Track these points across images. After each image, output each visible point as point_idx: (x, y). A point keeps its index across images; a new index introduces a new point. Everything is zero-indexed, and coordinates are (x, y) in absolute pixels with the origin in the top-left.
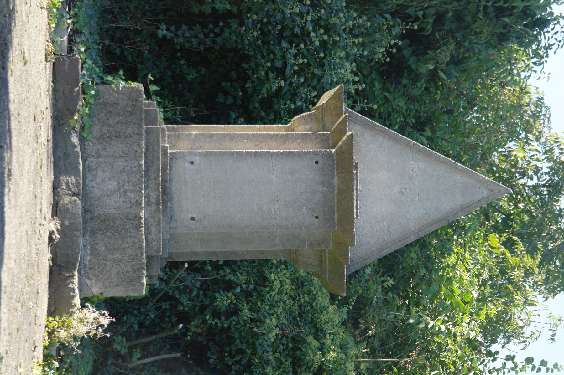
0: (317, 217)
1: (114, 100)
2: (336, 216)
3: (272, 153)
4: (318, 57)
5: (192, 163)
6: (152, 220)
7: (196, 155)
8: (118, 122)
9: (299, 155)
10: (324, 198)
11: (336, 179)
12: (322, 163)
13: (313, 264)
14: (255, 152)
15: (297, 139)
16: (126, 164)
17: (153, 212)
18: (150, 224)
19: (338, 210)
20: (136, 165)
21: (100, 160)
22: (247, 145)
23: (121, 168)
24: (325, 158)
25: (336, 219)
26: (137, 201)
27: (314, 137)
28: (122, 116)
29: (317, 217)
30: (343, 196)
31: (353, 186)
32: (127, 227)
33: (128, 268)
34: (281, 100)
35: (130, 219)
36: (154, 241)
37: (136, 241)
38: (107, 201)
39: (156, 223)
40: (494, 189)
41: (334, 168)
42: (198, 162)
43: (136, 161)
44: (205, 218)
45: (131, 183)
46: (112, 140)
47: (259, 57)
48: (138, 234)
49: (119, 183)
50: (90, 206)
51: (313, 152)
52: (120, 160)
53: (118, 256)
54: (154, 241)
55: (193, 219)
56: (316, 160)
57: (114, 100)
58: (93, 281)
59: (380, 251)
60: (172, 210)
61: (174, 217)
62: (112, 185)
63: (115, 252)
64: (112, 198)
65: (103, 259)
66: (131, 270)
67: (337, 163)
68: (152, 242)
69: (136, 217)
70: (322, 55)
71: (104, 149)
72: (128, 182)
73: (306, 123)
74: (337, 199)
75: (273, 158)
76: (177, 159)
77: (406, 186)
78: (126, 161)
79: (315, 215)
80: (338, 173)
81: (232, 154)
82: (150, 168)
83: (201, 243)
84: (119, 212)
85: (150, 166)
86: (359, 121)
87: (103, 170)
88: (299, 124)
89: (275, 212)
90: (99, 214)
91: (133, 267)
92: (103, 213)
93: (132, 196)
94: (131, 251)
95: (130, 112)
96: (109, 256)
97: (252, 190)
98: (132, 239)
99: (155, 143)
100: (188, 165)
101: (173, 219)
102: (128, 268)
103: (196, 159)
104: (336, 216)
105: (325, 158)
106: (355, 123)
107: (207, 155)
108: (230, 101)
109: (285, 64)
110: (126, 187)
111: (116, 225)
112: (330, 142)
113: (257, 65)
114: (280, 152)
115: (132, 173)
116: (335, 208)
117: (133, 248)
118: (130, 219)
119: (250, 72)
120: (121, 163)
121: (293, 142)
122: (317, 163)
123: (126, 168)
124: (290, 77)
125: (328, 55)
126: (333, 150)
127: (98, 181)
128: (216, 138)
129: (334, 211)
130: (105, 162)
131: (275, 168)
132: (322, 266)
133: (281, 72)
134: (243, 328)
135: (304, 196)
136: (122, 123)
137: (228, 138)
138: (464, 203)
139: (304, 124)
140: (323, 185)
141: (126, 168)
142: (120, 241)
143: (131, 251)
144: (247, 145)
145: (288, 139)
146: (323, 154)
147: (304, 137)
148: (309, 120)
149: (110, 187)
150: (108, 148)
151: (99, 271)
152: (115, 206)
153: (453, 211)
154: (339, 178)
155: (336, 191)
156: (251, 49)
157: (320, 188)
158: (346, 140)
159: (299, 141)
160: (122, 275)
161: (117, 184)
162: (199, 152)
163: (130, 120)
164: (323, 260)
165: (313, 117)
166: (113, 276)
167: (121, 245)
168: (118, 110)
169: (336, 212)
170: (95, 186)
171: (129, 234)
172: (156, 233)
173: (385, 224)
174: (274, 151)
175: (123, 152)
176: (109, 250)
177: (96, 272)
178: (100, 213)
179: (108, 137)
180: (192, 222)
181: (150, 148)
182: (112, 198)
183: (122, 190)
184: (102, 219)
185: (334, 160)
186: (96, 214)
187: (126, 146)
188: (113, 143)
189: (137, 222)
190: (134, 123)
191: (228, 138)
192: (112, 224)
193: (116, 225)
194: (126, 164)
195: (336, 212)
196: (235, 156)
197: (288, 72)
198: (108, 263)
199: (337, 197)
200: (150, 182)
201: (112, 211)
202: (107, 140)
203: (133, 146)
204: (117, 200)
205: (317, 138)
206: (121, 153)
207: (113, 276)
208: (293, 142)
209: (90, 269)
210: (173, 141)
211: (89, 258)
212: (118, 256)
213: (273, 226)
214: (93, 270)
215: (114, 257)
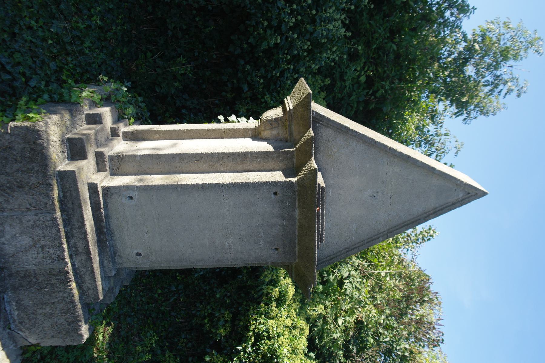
0: (276, 249)
1: (7, 144)
2: (297, 249)
4: (311, 13)
5: (131, 198)
6: (84, 270)
8: (18, 171)
10: (284, 231)
12: (281, 195)
16: (37, 218)
17: (83, 262)
18: (82, 273)
19: (299, 244)
20: (48, 218)
21: (5, 214)
22: (200, 166)
23: (32, 223)
25: (297, 252)
26: (59, 256)
27: (276, 155)
28: (21, 162)
29: (276, 249)
30: (305, 232)
31: (315, 227)
32: (53, 282)
33: (62, 321)
35: (54, 275)
36: (90, 289)
37: (65, 295)
38: (24, 258)
39: (89, 272)
40: (470, 192)
41: (295, 200)
43: (48, 215)
45: (47, 238)
46: (14, 191)
47: (259, 15)
48: (66, 289)
49: (33, 239)
50: (4, 263)
52: (29, 213)
53: (48, 310)
54: (90, 289)
55: (139, 254)
57: (7, 144)
58: (27, 334)
59: (347, 251)
60: (114, 246)
62: (26, 241)
63: (44, 307)
64: (28, 254)
65: (33, 313)
66: (65, 322)
68: (88, 291)
69: (60, 272)
70: (314, 12)
71: (7, 201)
72: (44, 237)
73: (273, 128)
74: (299, 232)
75: (224, 191)
77: (378, 191)
78: (36, 215)
79: (274, 248)
80: (299, 207)
82: (72, 216)
84: (40, 267)
85: (71, 214)
86: (331, 125)
87: (11, 225)
90: (18, 271)
91: (67, 320)
92: (22, 269)
93: (52, 251)
94: (62, 305)
95: (29, 157)
96: (38, 310)
97: (202, 225)
98: (61, 294)
99: (72, 189)
101: (117, 255)
102: (62, 321)
104: (297, 249)
105: (285, 189)
106: (327, 127)
108: (238, 51)
109: (280, 22)
110: (43, 242)
111: (40, 281)
112: (295, 160)
113: (258, 23)
115: (47, 227)
116: (297, 241)
117: (63, 302)
118: (54, 275)
119: (251, 29)
120: (31, 218)
121: (252, 161)
122: (275, 193)
123: (38, 223)
124: (286, 32)
125: (320, 11)
126: (294, 180)
127: (8, 236)
129: (294, 243)
130: (11, 216)
133: (278, 29)
136: (23, 172)
137: (178, 159)
138: (437, 205)
139: (270, 129)
140: (283, 217)
141: (38, 223)
142: (47, 297)
143: (62, 305)
144: (200, 166)
148: (276, 125)
149: (23, 243)
150: (11, 201)
151: (31, 324)
152: (34, 262)
153: (425, 213)
155: (297, 224)
156: (253, 7)
157: (279, 221)
160: (56, 327)
161: (31, 239)
163: (30, 167)
165: (280, 122)
166: (46, 329)
167: (49, 300)
168: (14, 155)
169: (297, 245)
170: (6, 242)
171: (56, 290)
172: (90, 281)
173: (354, 226)
175: (30, 205)
176: (37, 304)
177: (28, 325)
178: (19, 269)
179: (9, 188)
180: (138, 257)
181: (68, 194)
182: (28, 254)
183: (38, 246)
184: (22, 275)
186: (13, 271)
187: (33, 198)
188: (16, 194)
189: (63, 277)
190: (37, 171)
191: (178, 159)
192: (34, 280)
193: (40, 281)
194: (37, 218)
195: (297, 245)
196: (179, 189)
197: (283, 28)
198: (38, 317)
199: (298, 230)
200: (75, 231)
201: (32, 267)
202: (9, 191)
203: (41, 198)
204: (34, 256)
206: (28, 206)
207: (46, 329)
208: (252, 161)
209: (21, 323)
211: (16, 313)
212: (48, 310)
213: (228, 259)
214: (23, 324)
215: (44, 311)
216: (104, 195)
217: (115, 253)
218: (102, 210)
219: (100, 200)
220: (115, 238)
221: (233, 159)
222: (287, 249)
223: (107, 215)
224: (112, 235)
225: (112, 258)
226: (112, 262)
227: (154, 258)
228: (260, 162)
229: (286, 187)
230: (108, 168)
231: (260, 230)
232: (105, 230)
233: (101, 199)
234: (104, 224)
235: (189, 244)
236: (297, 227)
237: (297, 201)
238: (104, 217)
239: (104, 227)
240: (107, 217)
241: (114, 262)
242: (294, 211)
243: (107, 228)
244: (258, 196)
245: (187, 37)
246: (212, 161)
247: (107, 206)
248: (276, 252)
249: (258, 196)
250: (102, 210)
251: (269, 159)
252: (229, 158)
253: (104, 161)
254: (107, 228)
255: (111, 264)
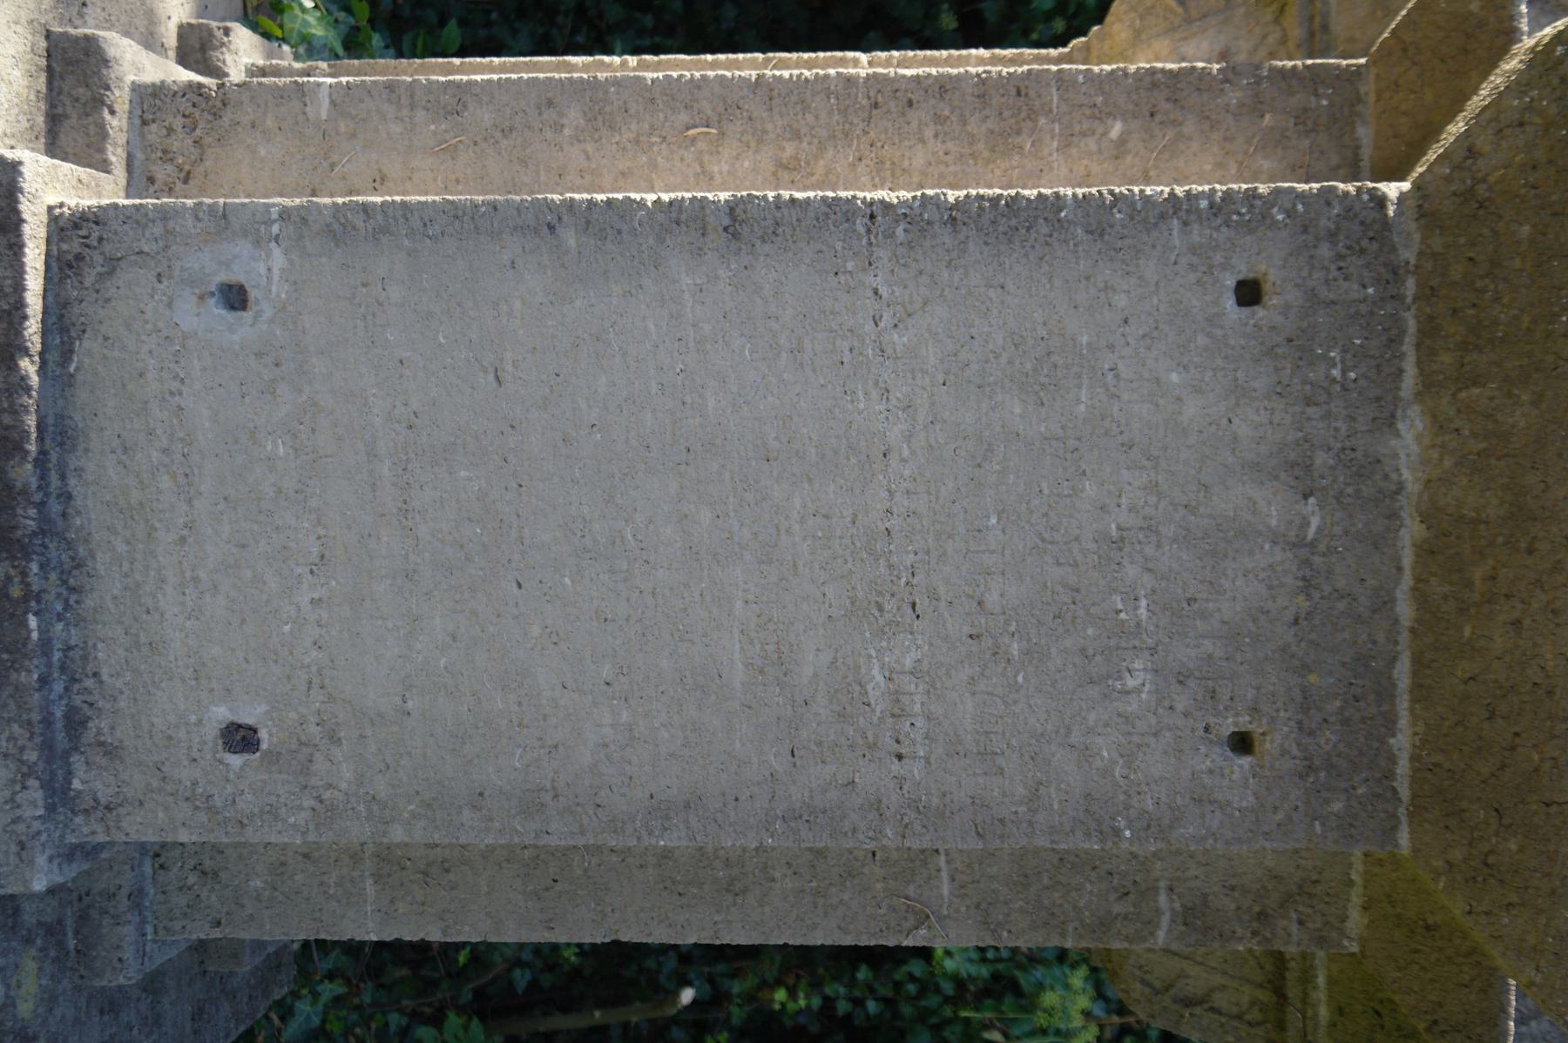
0: (1242, 743)
2: (1402, 741)
3: (875, 211)
5: (235, 297)
7: (256, 228)
9: (1098, 232)
10: (1307, 586)
11: (1412, 430)
12: (1294, 296)
13: (1220, 1000)
14: (732, 207)
15: (1101, 115)
19: (1420, 692)
22: (718, 168)
24: (1325, 251)
25: (1403, 767)
27: (1233, 97)
29: (1242, 743)
30: (1478, 574)
34: (1447, 588)
41: (1394, 341)
42: (279, 289)
44: (335, 740)
51: (1221, 208)
55: (240, 738)
56: (1244, 272)
60: (74, 667)
61: (99, 725)
67: (1427, 293)
73: (1189, 21)
74: (1420, 596)
75: (882, 254)
76: (113, 265)
79: (1228, 726)
80: (1429, 385)
81: (548, 223)
83: (377, 878)
88: (1137, 34)
89: (896, 696)
97: (706, 516)
100: (199, 318)
101: (89, 735)
103: (266, 270)
104: (1402, 741)
105: (1325, 251)
107: (342, 229)
114: (935, 202)
116: (1403, 673)
122: (1249, 293)
126: (1392, 190)
128: (486, 117)
129: (1386, 693)
131: (899, 340)
132: (1281, 1026)
134: (948, 1012)
135: (1131, 571)
137: (574, 117)
139: (1171, 30)
144: (718, 168)
145: (1032, 116)
146: (1305, 220)
147: (1162, 99)
154: (1439, 425)
155: (1411, 531)
157: (1273, 507)
158: (1520, 85)
159: (1116, 129)
162: (285, 214)
164: (1293, 992)
169: (1403, 704)
174: (892, 197)
180: (235, 760)
185: (1396, 272)
191: (574, 117)
195: (1403, 704)
196: (570, 238)
205: (1255, 107)
210: (180, 143)
213: (877, 806)
216: (60, 267)
217: (75, 723)
218: (29, 367)
219: (20, 288)
220: (89, 602)
221: (938, 119)
222: (1328, 738)
223: (60, 417)
224: (74, 575)
225: (48, 747)
226: (47, 786)
227: (347, 772)
228: (1122, 142)
229: (1332, 236)
230: (116, 156)
231: (1131, 571)
232: (28, 520)
233: (34, 283)
234: (24, 473)
235: (607, 671)
236: (1407, 560)
237: (1408, 347)
238: (31, 422)
239: (24, 492)
240: (60, 433)
241: (59, 796)
242: (1391, 421)
243: (43, 518)
244: (1121, 300)
245: (648, 20)
246: (797, 136)
247: (67, 354)
248: (1245, 761)
249: (1121, 300)
250: (29, 367)
251: (1190, 127)
252: (913, 116)
253: (98, 102)
254: (43, 518)
255: (35, 792)
